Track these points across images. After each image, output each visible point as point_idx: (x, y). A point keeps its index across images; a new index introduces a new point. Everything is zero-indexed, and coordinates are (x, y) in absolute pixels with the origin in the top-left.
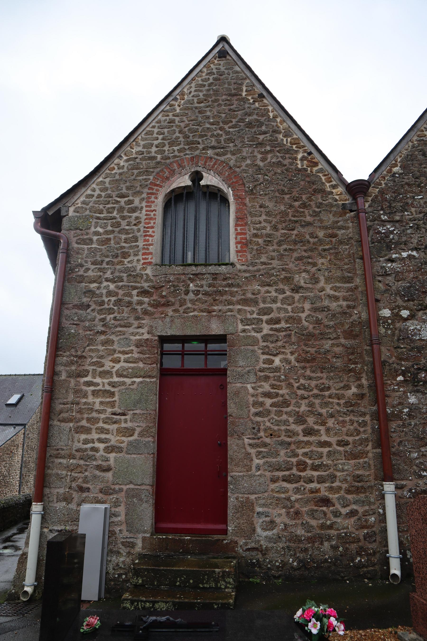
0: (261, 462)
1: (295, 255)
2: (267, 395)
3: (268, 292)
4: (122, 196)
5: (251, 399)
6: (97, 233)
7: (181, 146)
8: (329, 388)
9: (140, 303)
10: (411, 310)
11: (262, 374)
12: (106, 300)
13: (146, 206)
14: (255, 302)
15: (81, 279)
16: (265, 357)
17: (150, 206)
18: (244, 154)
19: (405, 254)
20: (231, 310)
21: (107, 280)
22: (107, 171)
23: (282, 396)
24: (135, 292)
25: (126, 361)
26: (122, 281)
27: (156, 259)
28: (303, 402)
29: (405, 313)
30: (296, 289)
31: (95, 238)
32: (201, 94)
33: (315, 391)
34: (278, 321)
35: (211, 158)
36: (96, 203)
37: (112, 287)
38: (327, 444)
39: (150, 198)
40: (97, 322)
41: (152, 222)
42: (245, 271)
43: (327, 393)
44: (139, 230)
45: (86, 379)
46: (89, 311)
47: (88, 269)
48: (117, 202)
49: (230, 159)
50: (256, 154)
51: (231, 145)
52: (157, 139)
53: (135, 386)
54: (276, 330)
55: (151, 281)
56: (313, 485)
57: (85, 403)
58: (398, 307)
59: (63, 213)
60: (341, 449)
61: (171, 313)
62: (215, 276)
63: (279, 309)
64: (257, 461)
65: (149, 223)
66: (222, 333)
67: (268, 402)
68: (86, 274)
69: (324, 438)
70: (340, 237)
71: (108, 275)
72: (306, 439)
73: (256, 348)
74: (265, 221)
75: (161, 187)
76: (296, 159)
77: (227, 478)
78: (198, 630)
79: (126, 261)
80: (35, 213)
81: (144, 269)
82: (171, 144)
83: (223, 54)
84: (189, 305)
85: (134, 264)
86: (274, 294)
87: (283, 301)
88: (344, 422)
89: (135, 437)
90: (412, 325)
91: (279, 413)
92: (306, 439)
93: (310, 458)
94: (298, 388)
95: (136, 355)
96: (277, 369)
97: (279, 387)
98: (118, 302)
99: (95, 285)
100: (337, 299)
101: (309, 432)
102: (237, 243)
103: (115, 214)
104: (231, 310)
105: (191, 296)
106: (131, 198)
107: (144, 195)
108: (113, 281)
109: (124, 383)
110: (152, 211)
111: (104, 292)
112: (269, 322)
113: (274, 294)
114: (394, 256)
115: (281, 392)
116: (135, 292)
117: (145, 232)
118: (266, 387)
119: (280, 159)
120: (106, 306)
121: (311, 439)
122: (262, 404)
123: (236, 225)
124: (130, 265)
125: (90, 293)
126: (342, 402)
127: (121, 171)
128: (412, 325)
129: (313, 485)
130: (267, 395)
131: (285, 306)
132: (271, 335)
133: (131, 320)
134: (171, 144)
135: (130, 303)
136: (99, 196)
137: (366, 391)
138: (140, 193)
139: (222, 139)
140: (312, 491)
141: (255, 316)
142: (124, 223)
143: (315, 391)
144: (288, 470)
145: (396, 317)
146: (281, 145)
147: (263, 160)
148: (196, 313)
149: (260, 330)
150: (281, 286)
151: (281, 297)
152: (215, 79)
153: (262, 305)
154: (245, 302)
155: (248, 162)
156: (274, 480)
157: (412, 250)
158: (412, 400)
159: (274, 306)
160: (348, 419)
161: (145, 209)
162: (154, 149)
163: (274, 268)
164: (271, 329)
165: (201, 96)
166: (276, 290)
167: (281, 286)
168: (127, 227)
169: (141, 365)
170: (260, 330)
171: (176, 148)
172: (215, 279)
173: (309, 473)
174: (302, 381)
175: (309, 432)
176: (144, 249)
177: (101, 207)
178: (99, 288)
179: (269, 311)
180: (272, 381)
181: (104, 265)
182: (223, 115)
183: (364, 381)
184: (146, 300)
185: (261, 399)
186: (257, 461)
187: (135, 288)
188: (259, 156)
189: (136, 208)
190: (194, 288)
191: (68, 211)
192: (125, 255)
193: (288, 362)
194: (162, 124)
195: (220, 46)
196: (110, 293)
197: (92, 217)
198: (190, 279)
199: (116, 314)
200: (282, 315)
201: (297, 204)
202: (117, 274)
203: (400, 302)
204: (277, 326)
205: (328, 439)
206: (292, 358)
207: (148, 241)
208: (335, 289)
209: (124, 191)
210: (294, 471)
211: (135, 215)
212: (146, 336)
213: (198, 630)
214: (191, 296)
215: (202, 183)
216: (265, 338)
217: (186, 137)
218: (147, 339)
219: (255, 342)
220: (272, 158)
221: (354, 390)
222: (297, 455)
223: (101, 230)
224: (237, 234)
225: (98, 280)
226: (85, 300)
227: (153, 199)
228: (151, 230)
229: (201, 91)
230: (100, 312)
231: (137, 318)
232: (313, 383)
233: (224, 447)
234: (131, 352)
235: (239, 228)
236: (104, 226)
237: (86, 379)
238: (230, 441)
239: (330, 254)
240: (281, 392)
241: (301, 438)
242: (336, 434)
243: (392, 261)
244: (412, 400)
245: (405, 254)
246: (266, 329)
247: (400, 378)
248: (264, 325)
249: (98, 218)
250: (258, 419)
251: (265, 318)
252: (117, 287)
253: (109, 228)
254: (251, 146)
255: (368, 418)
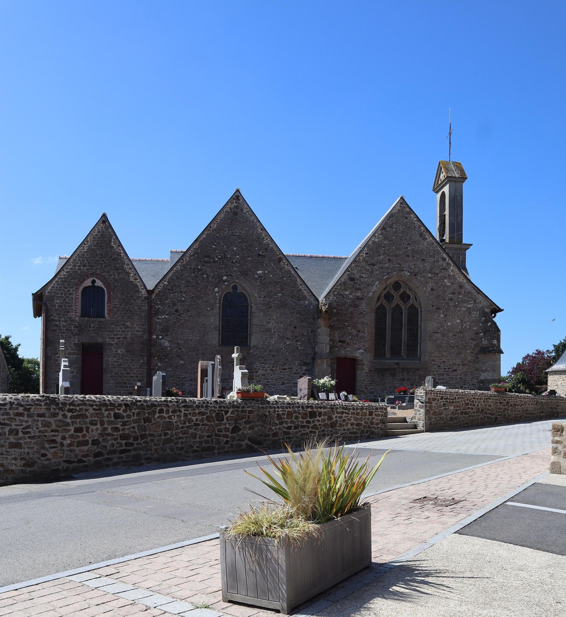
0: (113, 382)
1: (127, 315)
2: (115, 362)
3: (117, 328)
4: (66, 288)
5: (110, 363)
6: (57, 303)
7: (88, 267)
8: (134, 360)
9: (74, 330)
10: (163, 336)
11: (114, 355)
12: (63, 329)
13: (75, 293)
14: (113, 332)
15: (53, 320)
16: (115, 350)
17: (76, 294)
18: (111, 273)
19: (163, 317)
20: (105, 334)
21: (62, 321)
22: (59, 276)
23: (120, 362)
24: (72, 326)
25: (70, 350)
26: (68, 322)
27: (79, 314)
28: (126, 364)
29: (160, 337)
30: (127, 327)
31: (57, 305)
32: (95, 242)
33: (130, 361)
34: (120, 338)
35: (99, 274)
36: (55, 290)
37: (64, 324)
38: (133, 377)
39: (76, 290)
40: (60, 336)
41: (78, 300)
42: (110, 320)
43: (134, 362)
44: (73, 303)
45: (57, 356)
46: (57, 332)
47: (55, 317)
48: (64, 291)
49: (106, 275)
50: (115, 273)
51: (106, 269)
52: (78, 263)
53: (74, 358)
54: (119, 341)
55: (78, 322)
56: (128, 389)
57: (58, 363)
58: (159, 335)
59: (43, 294)
60: (137, 378)
61: (85, 334)
62: (100, 322)
63: (120, 335)
64: (111, 381)
65: (76, 300)
66: (358, 384)
67: (116, 364)
68: (54, 319)
69: (132, 375)
70: (142, 309)
71: (63, 319)
72: (126, 375)
73: (112, 347)
74: (117, 302)
75: (80, 285)
76: (130, 276)
77: (87, 317)
78: (92, 312)
79: (69, 314)
80: (33, 294)
81: (75, 318)
82: (84, 266)
83: (104, 222)
84: (91, 332)
85: (72, 316)
86: (119, 329)
87: (122, 331)
88: (138, 371)
89: (75, 374)
90: (163, 341)
91: (119, 368)
92: (126, 375)
93: (127, 381)
94: (125, 360)
95: (74, 348)
96: (119, 354)
97: (119, 360)
98: (67, 330)
99: (58, 323)
100: (139, 331)
101: (127, 373)
102: (107, 310)
103: (63, 295)
104: (105, 334)
105: (92, 328)
106: (69, 289)
107: (74, 289)
108: (64, 322)
109: (70, 357)
110: (77, 295)
111: (62, 325)
112: (117, 338)
113: (119, 329)
114: (160, 317)
115: (119, 361)
116: (72, 326)
117: (75, 304)
118: (115, 359)
119: (124, 276)
120: (63, 331)
121: (128, 375)
122: (114, 364)
123: (107, 303)
124: (70, 316)
125: (56, 325)
126: (138, 364)
127: (65, 277)
128: (163, 341)
129: (128, 389)
130: (115, 362)
131: (122, 333)
132: (117, 343)
133: (72, 336)
134: (84, 266)
135: (71, 330)
136: (57, 287)
137: (145, 362)
138: (72, 287)
139: (103, 265)
140: (127, 390)
141: (112, 336)
142: (67, 300)
143: (130, 361)
144: (121, 384)
145: (158, 338)
146: (125, 270)
147: (118, 276)
148: (93, 335)
149: (114, 341)
150: (122, 327)
151: (121, 330)
152: (101, 235)
153: (115, 333)
154: (110, 331)
155: (113, 277)
156: (117, 387)
157: (166, 315)
158: (159, 365)
159: (119, 333)
160: (139, 370)
161: (74, 294)
162: (77, 268)
163: (119, 320)
164: (118, 341)
165: (95, 244)
166: (120, 328)
167: (122, 327)
168: (68, 301)
169: (76, 351)
170: (114, 341)
171: (85, 268)
172: (99, 323)
173: (127, 385)
174: (126, 358)
175: (127, 373)
176: (75, 310)
177: (58, 292)
178: (60, 324)
179: (117, 335)
180: (117, 358)
181: (61, 316)
182: (104, 254)
183: (145, 359)
184: (77, 329)
185: (113, 363)
186: (111, 381)
187: (72, 325)
188: (117, 275)
189: (71, 293)
190: (93, 326)
191: (45, 293)
192: (68, 312)
193: (122, 351)
194: (80, 256)
195: (103, 218)
196: (64, 326)
197: (55, 296)
198: (91, 322)
199: (66, 334)
200: (121, 336)
201: (129, 295)
202: (66, 319)
203: (159, 333)
204: (120, 340)
205: (133, 375)
206: (124, 351)
207: (76, 307)
208: (139, 328)
209: (66, 286)
210: (123, 384)
211: (71, 296)
212: (77, 342)
213: (92, 312)
214: (92, 328)
215: (96, 284)
216: (116, 344)
217: (89, 263)
218: (77, 343)
219: (112, 345)
220: (121, 275)
221: (142, 361)
222: (124, 380)
223: (59, 302)
224: (108, 307)
225: (59, 321)
226: (55, 328)
227: (77, 291)
228: (77, 303)
229: (95, 241)
230: (61, 333)
231: (74, 336)
232: (130, 358)
233: (102, 377)
234: (72, 347)
235: (108, 304)
236: (60, 300)
237: (57, 356)
238: (104, 375)
239: (139, 315)
240: (119, 361)
241: (125, 375)
242: (135, 374)
243: (159, 319)
244: (159, 365)
245: (163, 317)
246: (116, 341)
247: (156, 358)
248: (115, 339)
249: (57, 297)
250: (112, 369)
251: (116, 337)
252: (66, 324)
253: (62, 301)
254: (114, 269)
255: (145, 370)
